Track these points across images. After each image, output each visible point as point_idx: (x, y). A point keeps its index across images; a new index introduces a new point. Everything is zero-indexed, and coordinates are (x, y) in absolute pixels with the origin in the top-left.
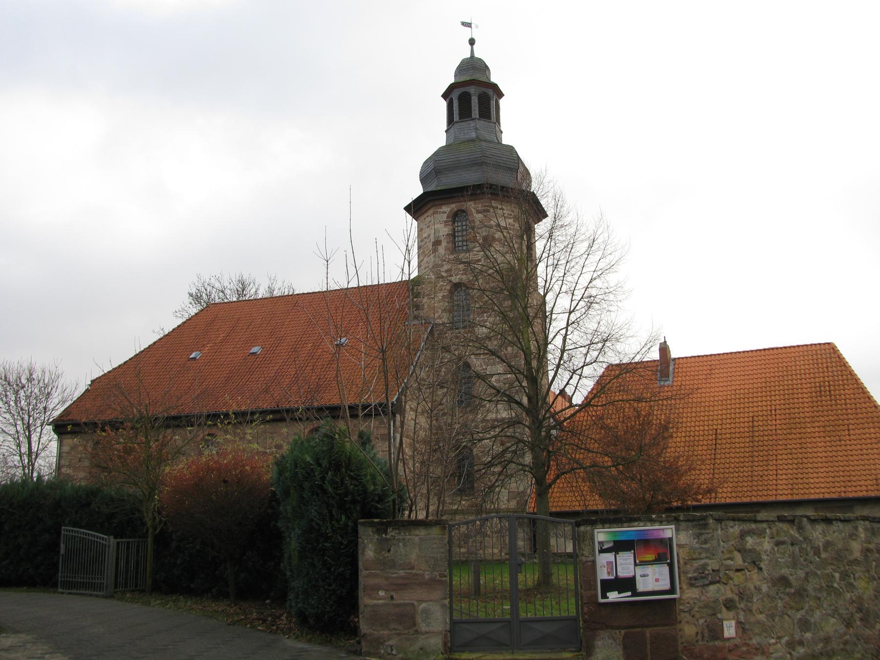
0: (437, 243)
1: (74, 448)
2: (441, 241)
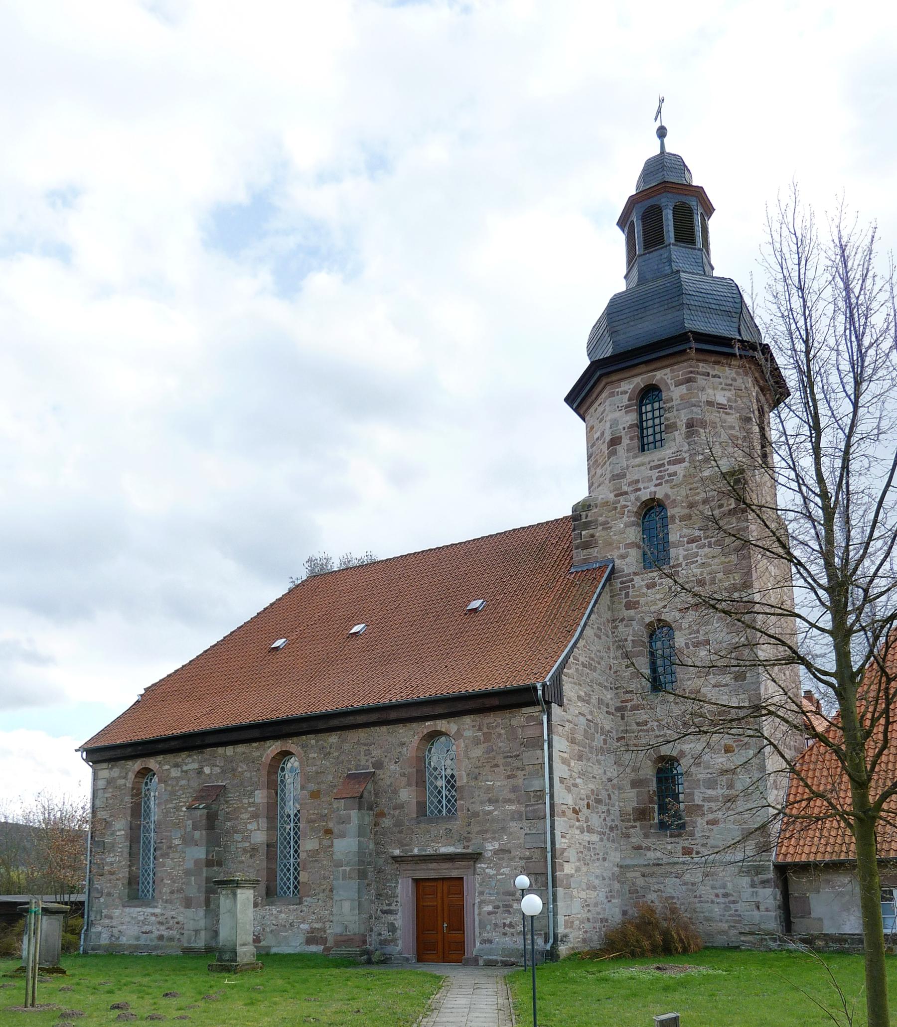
0: (615, 442)
1: (110, 782)
2: (621, 437)
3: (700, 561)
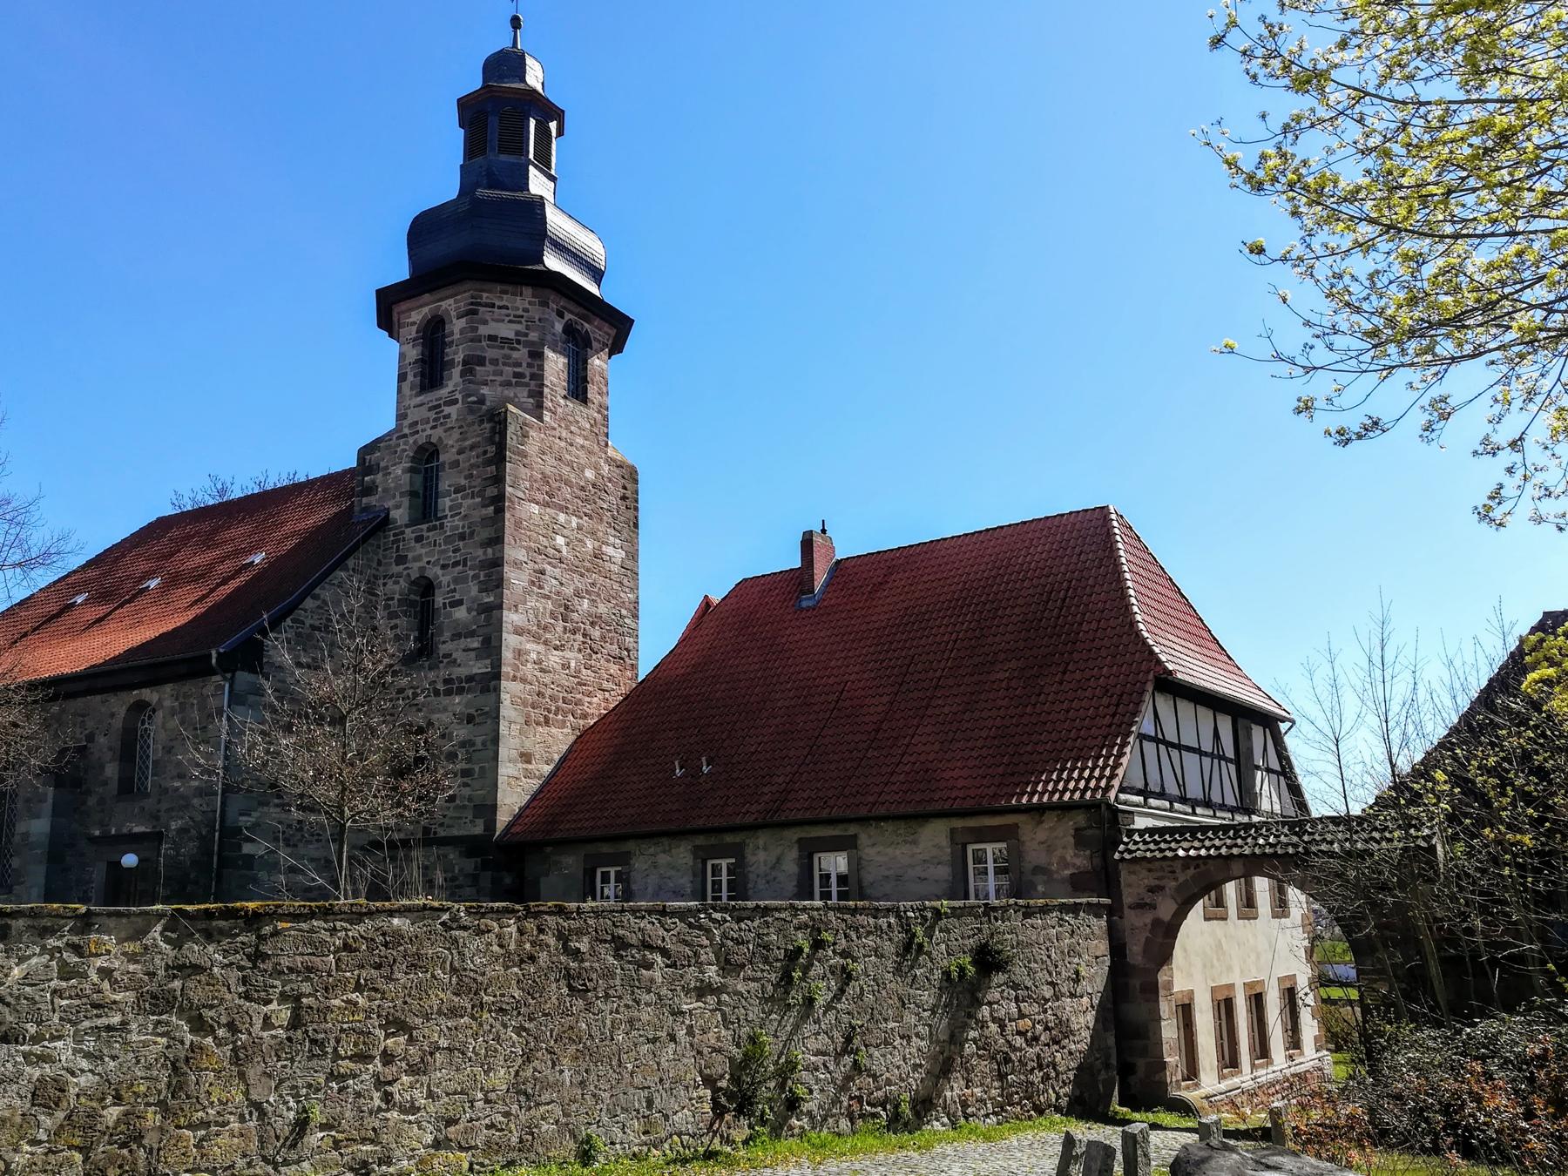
3: (463, 513)
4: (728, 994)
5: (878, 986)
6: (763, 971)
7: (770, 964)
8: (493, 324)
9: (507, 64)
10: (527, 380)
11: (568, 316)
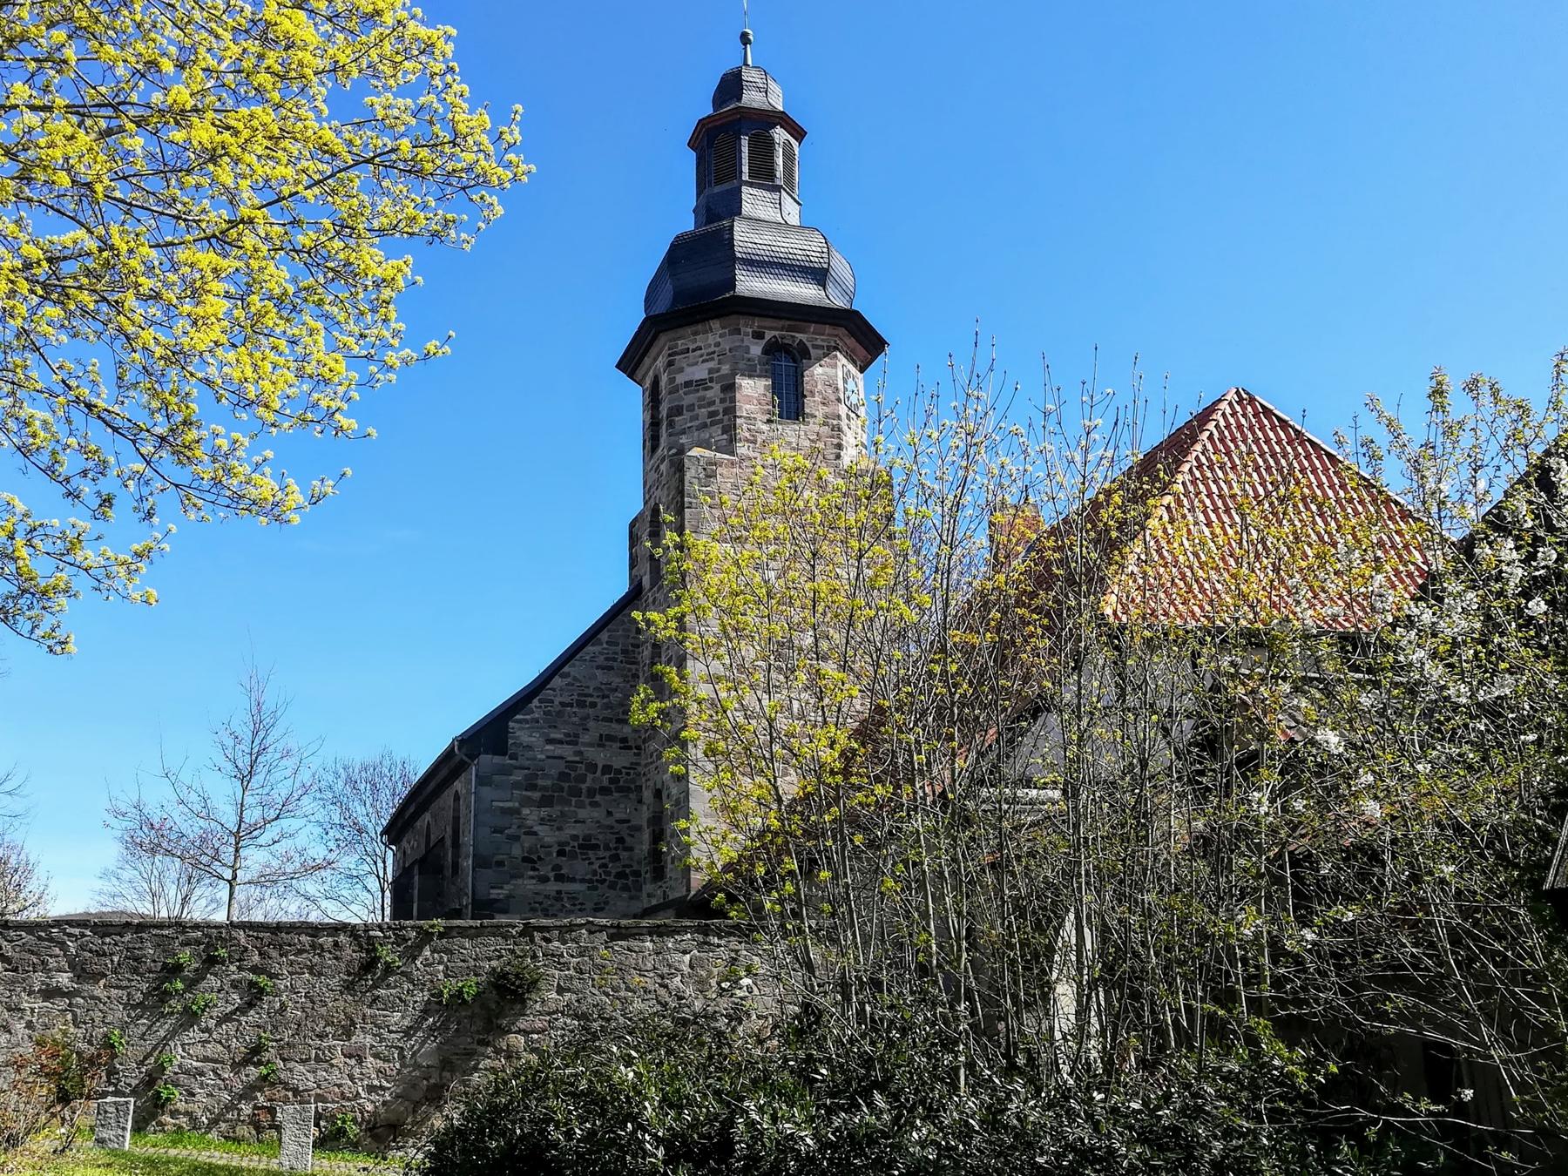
4: (83, 998)
5: (313, 1003)
6: (129, 980)
7: (141, 975)
8: (689, 370)
9: (731, 85)
10: (720, 416)
11: (769, 335)
